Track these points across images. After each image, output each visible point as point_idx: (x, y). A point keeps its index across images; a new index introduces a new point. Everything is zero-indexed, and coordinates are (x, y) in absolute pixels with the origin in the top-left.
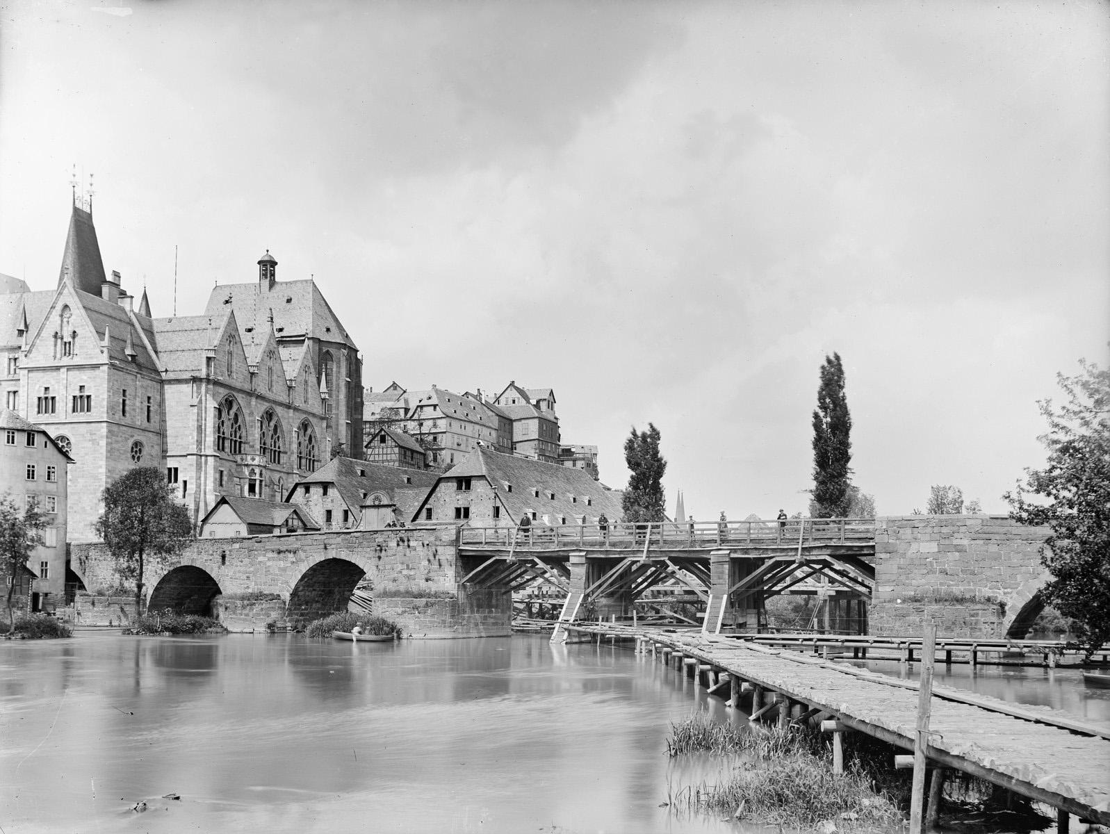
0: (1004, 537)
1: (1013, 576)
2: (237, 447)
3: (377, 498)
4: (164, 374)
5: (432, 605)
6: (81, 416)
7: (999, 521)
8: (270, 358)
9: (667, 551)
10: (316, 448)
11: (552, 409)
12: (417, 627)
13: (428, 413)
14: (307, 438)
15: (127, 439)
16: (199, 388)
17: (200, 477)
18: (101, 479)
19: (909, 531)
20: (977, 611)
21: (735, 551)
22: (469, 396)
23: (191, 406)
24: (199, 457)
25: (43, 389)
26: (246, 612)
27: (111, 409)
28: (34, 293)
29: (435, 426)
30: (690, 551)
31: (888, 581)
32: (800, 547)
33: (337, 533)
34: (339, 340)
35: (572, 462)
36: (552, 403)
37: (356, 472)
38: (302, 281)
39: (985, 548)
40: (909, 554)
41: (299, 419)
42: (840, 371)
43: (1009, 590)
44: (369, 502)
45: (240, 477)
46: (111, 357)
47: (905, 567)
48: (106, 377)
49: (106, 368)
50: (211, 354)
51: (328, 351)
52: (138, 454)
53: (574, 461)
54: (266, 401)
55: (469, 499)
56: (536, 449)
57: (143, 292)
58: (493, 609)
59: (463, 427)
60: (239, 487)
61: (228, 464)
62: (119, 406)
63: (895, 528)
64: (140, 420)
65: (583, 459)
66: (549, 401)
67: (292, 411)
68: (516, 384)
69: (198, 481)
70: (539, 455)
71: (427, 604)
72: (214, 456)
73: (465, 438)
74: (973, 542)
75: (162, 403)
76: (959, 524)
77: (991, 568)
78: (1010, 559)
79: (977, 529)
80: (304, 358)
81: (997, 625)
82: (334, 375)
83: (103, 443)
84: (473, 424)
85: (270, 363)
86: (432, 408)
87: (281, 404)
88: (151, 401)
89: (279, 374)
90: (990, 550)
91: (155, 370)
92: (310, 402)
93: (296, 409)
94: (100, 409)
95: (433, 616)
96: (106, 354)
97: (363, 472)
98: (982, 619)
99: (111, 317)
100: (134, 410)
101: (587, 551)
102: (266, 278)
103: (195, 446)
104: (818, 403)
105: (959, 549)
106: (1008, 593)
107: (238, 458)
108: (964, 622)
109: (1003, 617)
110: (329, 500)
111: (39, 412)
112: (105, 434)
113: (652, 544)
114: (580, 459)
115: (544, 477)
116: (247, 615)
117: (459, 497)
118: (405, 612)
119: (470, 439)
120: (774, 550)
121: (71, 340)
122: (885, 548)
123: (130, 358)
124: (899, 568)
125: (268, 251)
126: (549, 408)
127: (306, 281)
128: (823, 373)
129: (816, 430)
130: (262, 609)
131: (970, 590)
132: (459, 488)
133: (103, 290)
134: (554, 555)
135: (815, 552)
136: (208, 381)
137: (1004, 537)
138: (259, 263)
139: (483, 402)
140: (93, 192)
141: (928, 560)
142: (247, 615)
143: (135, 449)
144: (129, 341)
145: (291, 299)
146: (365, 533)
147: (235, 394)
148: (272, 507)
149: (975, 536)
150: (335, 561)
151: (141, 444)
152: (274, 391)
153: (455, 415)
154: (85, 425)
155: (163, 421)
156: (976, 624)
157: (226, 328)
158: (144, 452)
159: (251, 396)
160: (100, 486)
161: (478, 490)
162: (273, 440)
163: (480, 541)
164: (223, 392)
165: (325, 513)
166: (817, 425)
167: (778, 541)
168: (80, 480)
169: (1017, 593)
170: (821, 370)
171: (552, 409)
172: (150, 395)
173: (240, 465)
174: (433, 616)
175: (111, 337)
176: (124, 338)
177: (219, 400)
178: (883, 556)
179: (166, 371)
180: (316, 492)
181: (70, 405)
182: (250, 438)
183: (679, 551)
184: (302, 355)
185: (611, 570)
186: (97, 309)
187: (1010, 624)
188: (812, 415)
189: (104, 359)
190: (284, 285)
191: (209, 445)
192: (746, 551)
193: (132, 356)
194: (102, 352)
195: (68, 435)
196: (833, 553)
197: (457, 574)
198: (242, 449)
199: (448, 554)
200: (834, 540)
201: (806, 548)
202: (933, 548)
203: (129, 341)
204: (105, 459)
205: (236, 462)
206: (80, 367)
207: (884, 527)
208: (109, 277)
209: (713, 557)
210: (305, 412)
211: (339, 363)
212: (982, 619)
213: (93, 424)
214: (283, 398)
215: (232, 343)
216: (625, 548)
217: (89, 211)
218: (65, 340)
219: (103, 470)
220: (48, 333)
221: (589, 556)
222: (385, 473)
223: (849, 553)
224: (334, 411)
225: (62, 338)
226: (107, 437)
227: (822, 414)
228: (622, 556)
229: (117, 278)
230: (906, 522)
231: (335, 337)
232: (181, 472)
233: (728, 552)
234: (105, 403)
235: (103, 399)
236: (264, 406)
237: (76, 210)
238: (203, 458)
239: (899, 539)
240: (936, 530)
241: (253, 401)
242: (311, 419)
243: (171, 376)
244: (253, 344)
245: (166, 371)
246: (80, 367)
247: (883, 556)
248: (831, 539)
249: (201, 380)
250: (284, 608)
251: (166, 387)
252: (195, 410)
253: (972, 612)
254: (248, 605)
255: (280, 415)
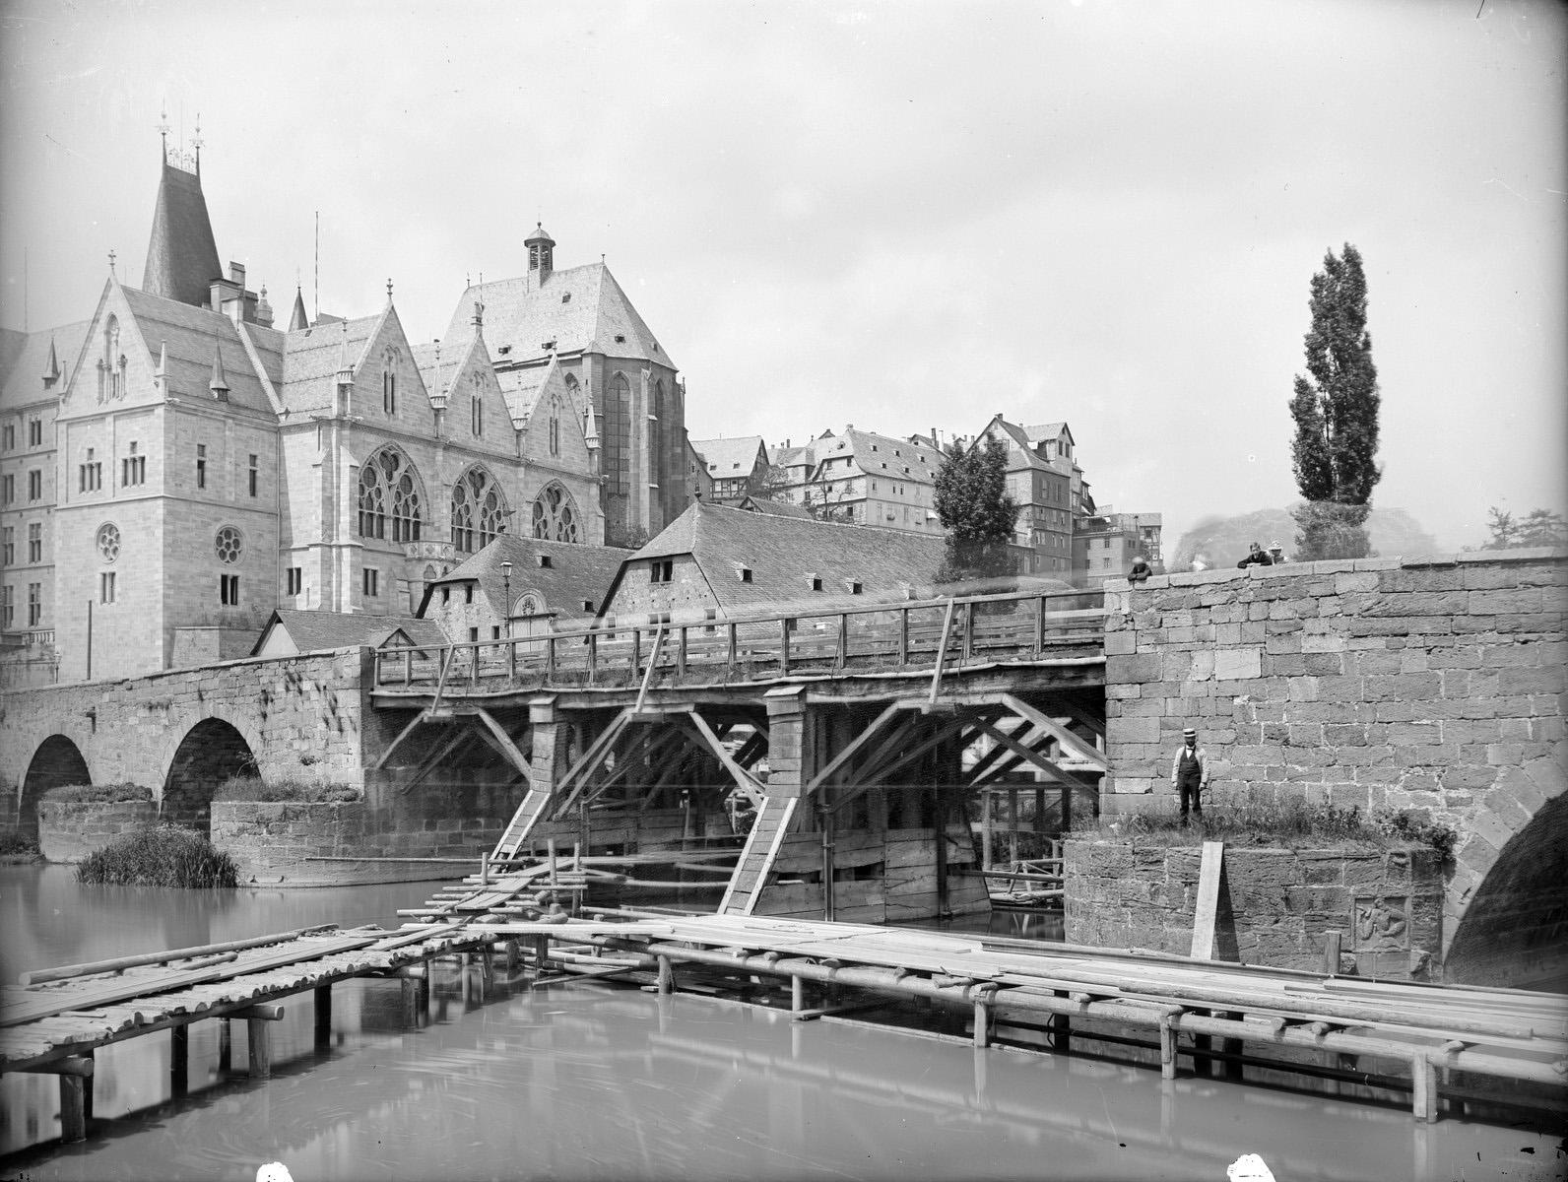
0: (1444, 625)
1: (1474, 749)
2: (412, 529)
3: (528, 604)
4: (284, 417)
5: (297, 815)
6: (133, 492)
7: (1431, 574)
8: (478, 384)
9: (691, 690)
10: (579, 530)
11: (1067, 456)
12: (266, 863)
13: (839, 469)
14: (559, 513)
15: (206, 525)
16: (328, 436)
17: (329, 583)
18: (157, 591)
19: (1186, 618)
20: (1333, 864)
21: (814, 686)
22: (920, 442)
23: (315, 466)
24: (327, 549)
25: (86, 452)
26: (71, 823)
27: (173, 475)
28: (274, 332)
29: (849, 490)
30: (730, 690)
31: (1139, 764)
32: (935, 672)
33: (214, 668)
34: (638, 353)
35: (1102, 541)
36: (1067, 445)
37: (535, 561)
38: (587, 267)
39: (1389, 662)
40: (1187, 686)
41: (541, 482)
42: (1359, 284)
43: (1463, 793)
44: (518, 612)
45: (411, 579)
46: (171, 393)
47: (1179, 724)
48: (163, 425)
49: (160, 411)
50: (347, 380)
51: (620, 374)
52: (232, 549)
53: (1107, 538)
54: (468, 454)
55: (669, 599)
56: (1029, 521)
57: (296, 296)
58: (482, 821)
59: (898, 491)
60: (407, 596)
61: (387, 559)
62: (190, 472)
63: (1152, 610)
64: (237, 492)
65: (1121, 534)
66: (1061, 443)
67: (523, 469)
68: (1004, 419)
69: (327, 589)
70: (1034, 531)
71: (285, 813)
72: (352, 546)
73: (902, 508)
74: (1355, 645)
75: (279, 466)
76: (1316, 590)
77: (1409, 723)
78: (1463, 694)
79: (1369, 604)
80: (549, 382)
81: (1417, 906)
82: (632, 411)
83: (159, 532)
84: (916, 485)
85: (477, 393)
86: (845, 461)
87: (500, 459)
88: (258, 462)
89: (497, 409)
90: (1406, 668)
91: (267, 413)
92: (563, 454)
93: (529, 466)
94: (155, 480)
95: (299, 837)
96: (161, 388)
97: (546, 561)
98: (1352, 890)
99: (195, 331)
100: (222, 477)
101: (559, 694)
102: (536, 267)
103: (320, 532)
104: (1305, 361)
105: (1318, 666)
106: (1460, 802)
107: (408, 548)
108: (1286, 899)
109: (1448, 881)
110: (474, 611)
111: (83, 489)
112: (161, 517)
113: (663, 675)
114: (1116, 535)
115: (851, 554)
116: (73, 829)
117: (654, 595)
118: (242, 830)
119: (912, 510)
120: (893, 682)
121: (119, 370)
122: (1128, 670)
123: (216, 395)
124: (1164, 726)
125: (539, 224)
126: (1061, 453)
127: (594, 266)
128: (1315, 293)
129: (1299, 420)
130: (101, 818)
131: (1353, 793)
132: (655, 578)
133: (212, 294)
134: (508, 703)
135: (978, 686)
136: (341, 422)
137: (1444, 625)
138: (527, 243)
139: (941, 449)
140: (201, 142)
141: (1237, 701)
142: (73, 829)
143: (225, 541)
144: (215, 367)
145: (569, 296)
146: (247, 667)
147: (402, 444)
148: (373, 626)
149: (1363, 626)
150: (212, 721)
151: (237, 532)
152: (487, 438)
153: (884, 472)
154: (136, 504)
155: (282, 493)
156: (1328, 903)
157: (379, 336)
158: (244, 546)
159: (435, 447)
160: (156, 601)
161: (683, 581)
162: (488, 518)
163: (399, 678)
164: (374, 442)
165: (469, 633)
166: (1302, 410)
167: (901, 660)
168: (131, 593)
169: (1488, 803)
170: (1312, 288)
171: (1067, 456)
172: (253, 453)
173: (410, 560)
174: (299, 837)
175: (170, 357)
176: (210, 363)
177: (366, 454)
178: (1123, 692)
179: (287, 412)
180: (458, 594)
181: (120, 474)
182: (435, 516)
183: (710, 690)
184: (541, 383)
185: (598, 736)
186: (169, 319)
187: (1467, 901)
188: (1294, 386)
189: (159, 395)
190: (563, 276)
191: (345, 534)
192: (835, 685)
193: (218, 390)
194: (157, 385)
195: (117, 523)
196: (1019, 686)
197: (367, 748)
198: (421, 534)
199: (350, 703)
200: (1023, 652)
201: (954, 675)
202: (1248, 664)
203: (215, 367)
204: (161, 558)
205: (405, 555)
206: (130, 412)
207: (1125, 611)
208: (227, 274)
209: (772, 702)
210: (553, 471)
211: (638, 391)
212: (1352, 890)
213: (146, 503)
214: (508, 448)
215: (394, 360)
216: (619, 685)
217: (194, 172)
218: (114, 371)
219: (159, 576)
220: (90, 364)
221: (563, 706)
222: (599, 560)
223: (1056, 684)
224: (632, 471)
225: (110, 369)
226: (165, 522)
227: (1312, 381)
228: (615, 704)
229: (239, 274)
230: (1178, 593)
231: (633, 350)
232: (306, 574)
233: (797, 689)
234: (161, 467)
235: (159, 461)
236: (461, 465)
237: (168, 170)
238: (334, 550)
239: (1160, 643)
240: (1257, 610)
241: (440, 455)
242: (565, 482)
243: (292, 420)
244: (437, 364)
245: (287, 412)
246: (130, 412)
247: (1123, 692)
248: (1015, 648)
249: (329, 422)
250: (152, 816)
251: (285, 438)
252: (319, 472)
253: (1313, 867)
254: (74, 811)
255: (498, 477)
